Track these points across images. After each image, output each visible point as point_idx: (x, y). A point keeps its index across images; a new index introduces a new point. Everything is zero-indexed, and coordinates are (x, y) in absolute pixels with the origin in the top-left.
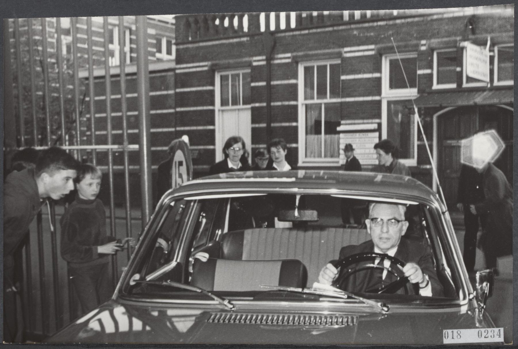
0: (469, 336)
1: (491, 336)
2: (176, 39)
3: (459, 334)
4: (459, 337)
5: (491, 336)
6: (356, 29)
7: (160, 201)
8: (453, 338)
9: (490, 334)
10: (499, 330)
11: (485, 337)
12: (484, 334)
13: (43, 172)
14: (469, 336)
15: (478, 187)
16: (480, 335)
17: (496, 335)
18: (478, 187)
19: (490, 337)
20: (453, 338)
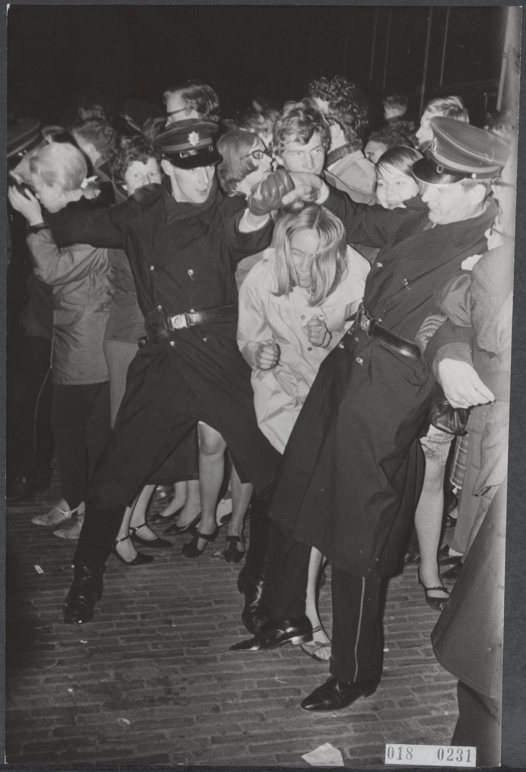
0: (424, 755)
1: (457, 758)
2: (155, 116)
3: (410, 753)
4: (409, 756)
5: (457, 758)
6: (282, 672)
7: (509, 173)
8: (468, 761)
9: (456, 755)
10: (400, 749)
11: (448, 760)
12: (446, 755)
13: (438, 362)
14: (424, 755)
15: (191, 272)
16: (440, 755)
17: (466, 756)
18: (191, 272)
19: (455, 760)
20: (400, 758)
